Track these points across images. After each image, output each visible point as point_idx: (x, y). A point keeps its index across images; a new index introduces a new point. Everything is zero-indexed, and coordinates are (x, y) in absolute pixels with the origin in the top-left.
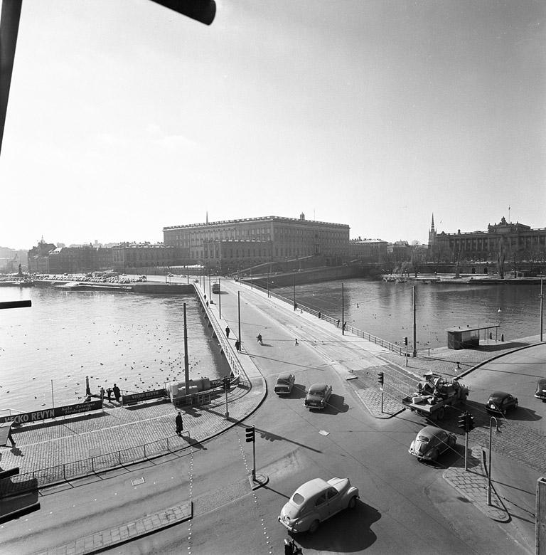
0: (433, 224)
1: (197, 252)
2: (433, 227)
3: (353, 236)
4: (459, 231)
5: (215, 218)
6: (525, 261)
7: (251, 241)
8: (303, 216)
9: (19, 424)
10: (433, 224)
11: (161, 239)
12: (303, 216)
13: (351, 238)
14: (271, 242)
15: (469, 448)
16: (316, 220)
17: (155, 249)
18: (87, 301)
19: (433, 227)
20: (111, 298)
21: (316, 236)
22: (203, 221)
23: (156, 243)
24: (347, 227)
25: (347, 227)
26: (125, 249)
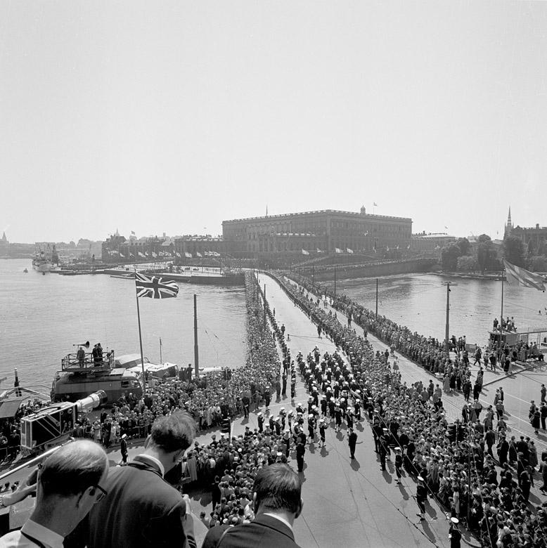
0: (509, 217)
1: (254, 246)
2: (509, 221)
3: (415, 230)
4: (538, 225)
5: (273, 213)
6: (122, 256)
7: (300, 235)
8: (363, 209)
9: (482, 427)
10: (509, 217)
11: (501, 237)
12: (363, 209)
13: (414, 232)
14: (327, 237)
15: (46, 396)
16: (375, 214)
17: (214, 242)
18: (398, 301)
19: (509, 221)
20: (108, 276)
21: (375, 230)
22: (263, 215)
23: (217, 237)
24: (409, 222)
25: (409, 222)
26: (186, 242)
